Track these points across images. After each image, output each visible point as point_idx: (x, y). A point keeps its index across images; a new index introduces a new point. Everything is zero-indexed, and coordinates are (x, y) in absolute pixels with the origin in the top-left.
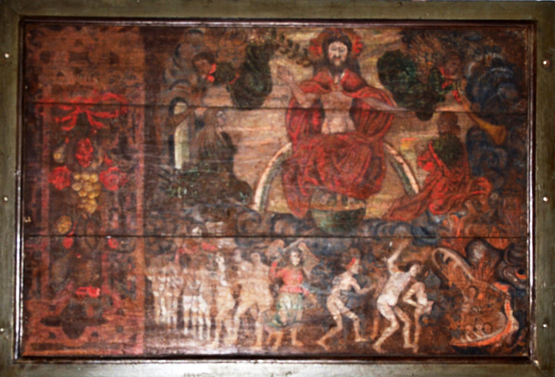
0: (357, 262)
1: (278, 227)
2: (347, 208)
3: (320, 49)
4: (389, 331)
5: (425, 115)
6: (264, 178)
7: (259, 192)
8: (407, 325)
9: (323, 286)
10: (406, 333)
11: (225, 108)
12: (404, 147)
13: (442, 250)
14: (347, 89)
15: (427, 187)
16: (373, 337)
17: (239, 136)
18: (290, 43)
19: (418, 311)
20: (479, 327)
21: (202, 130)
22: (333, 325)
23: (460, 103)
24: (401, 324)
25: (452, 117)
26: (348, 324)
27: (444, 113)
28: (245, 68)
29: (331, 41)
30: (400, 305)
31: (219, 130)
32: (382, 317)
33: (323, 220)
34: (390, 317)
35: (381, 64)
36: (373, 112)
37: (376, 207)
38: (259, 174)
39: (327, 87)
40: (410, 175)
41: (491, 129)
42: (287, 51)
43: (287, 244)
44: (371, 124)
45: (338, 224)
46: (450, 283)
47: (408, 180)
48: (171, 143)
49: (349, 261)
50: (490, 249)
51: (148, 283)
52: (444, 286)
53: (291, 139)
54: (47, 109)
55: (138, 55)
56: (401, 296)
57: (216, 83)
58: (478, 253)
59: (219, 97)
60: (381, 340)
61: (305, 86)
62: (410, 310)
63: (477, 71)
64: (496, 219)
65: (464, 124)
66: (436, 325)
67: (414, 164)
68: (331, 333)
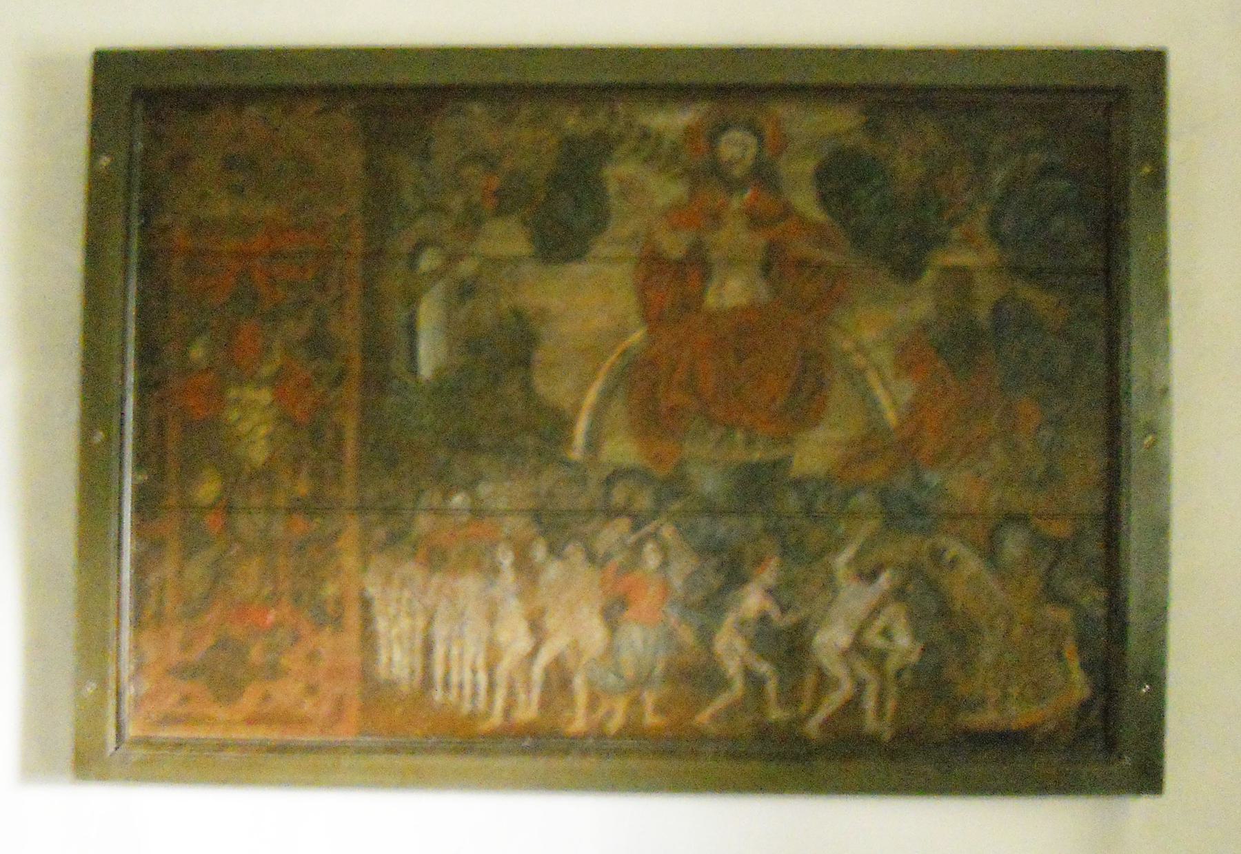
0: (774, 563)
1: (619, 496)
2: (756, 456)
3: (702, 143)
4: (834, 700)
5: (909, 270)
6: (592, 397)
7: (582, 426)
8: (871, 690)
9: (711, 606)
10: (870, 704)
11: (517, 260)
12: (868, 335)
13: (943, 541)
17: (542, 313)
18: (645, 135)
19: (892, 664)
20: (1014, 691)
21: (470, 304)
22: (725, 684)
23: (979, 249)
24: (860, 686)
25: (961, 279)
26: (755, 682)
27: (946, 270)
28: (556, 180)
29: (725, 128)
30: (858, 647)
31: (505, 304)
32: (822, 675)
33: (709, 482)
34: (837, 670)
35: (822, 175)
37: (814, 453)
38: (582, 389)
39: (716, 218)
40: (879, 392)
41: (1041, 301)
43: (636, 527)
46: (958, 607)
47: (875, 402)
48: (411, 330)
49: (759, 561)
50: (1039, 541)
51: (366, 604)
52: (945, 612)
53: (646, 319)
54: (178, 262)
56: (859, 633)
57: (500, 212)
58: (1013, 545)
59: (507, 239)
60: (822, 714)
61: (676, 216)
63: (1009, 191)
64: (1050, 476)
65: (987, 291)
66: (930, 682)
67: (889, 373)
68: (721, 701)
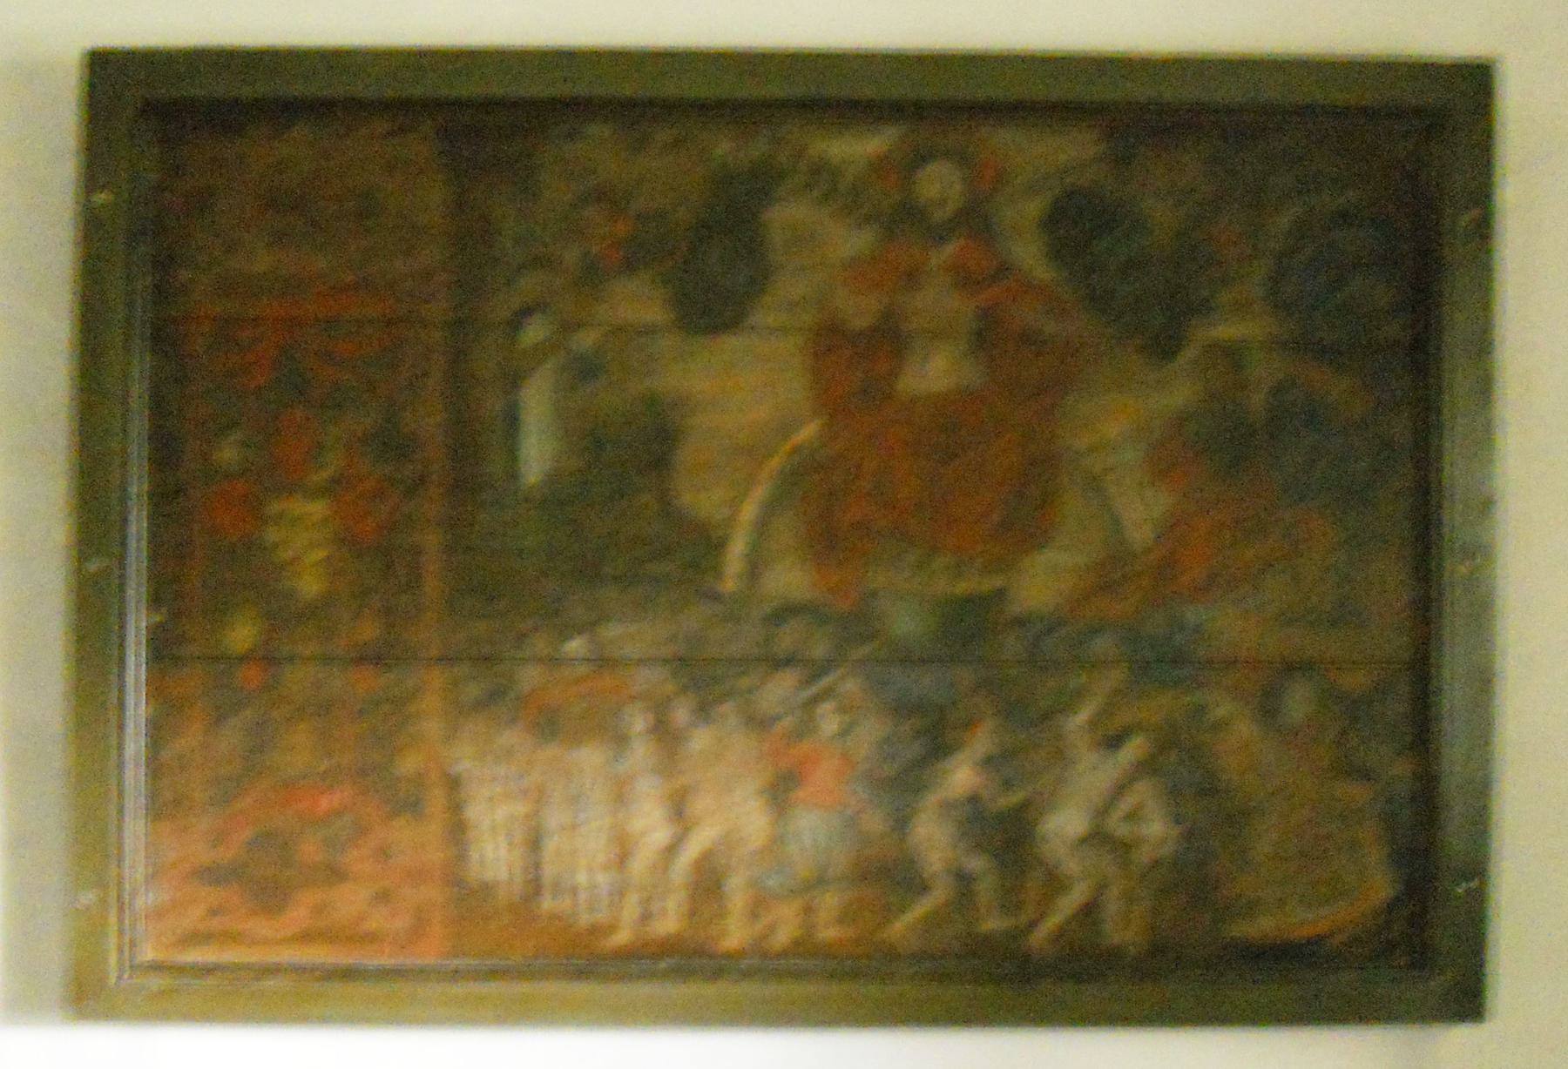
5: (1164, 347)
11: (649, 331)
14: (965, 279)
15: (1172, 527)
16: (1023, 919)
25: (1231, 355)
26: (964, 880)
30: (1097, 837)
33: (906, 622)
34: (1071, 866)
35: (1054, 219)
36: (1027, 338)
39: (912, 278)
42: (809, 186)
44: (1026, 373)
45: (641, 752)
48: (512, 421)
49: (969, 724)
52: (1209, 789)
55: (432, 199)
56: (1103, 812)
57: (629, 267)
58: (1299, 702)
59: (638, 302)
62: (1122, 848)
66: (1191, 881)
68: (921, 908)
